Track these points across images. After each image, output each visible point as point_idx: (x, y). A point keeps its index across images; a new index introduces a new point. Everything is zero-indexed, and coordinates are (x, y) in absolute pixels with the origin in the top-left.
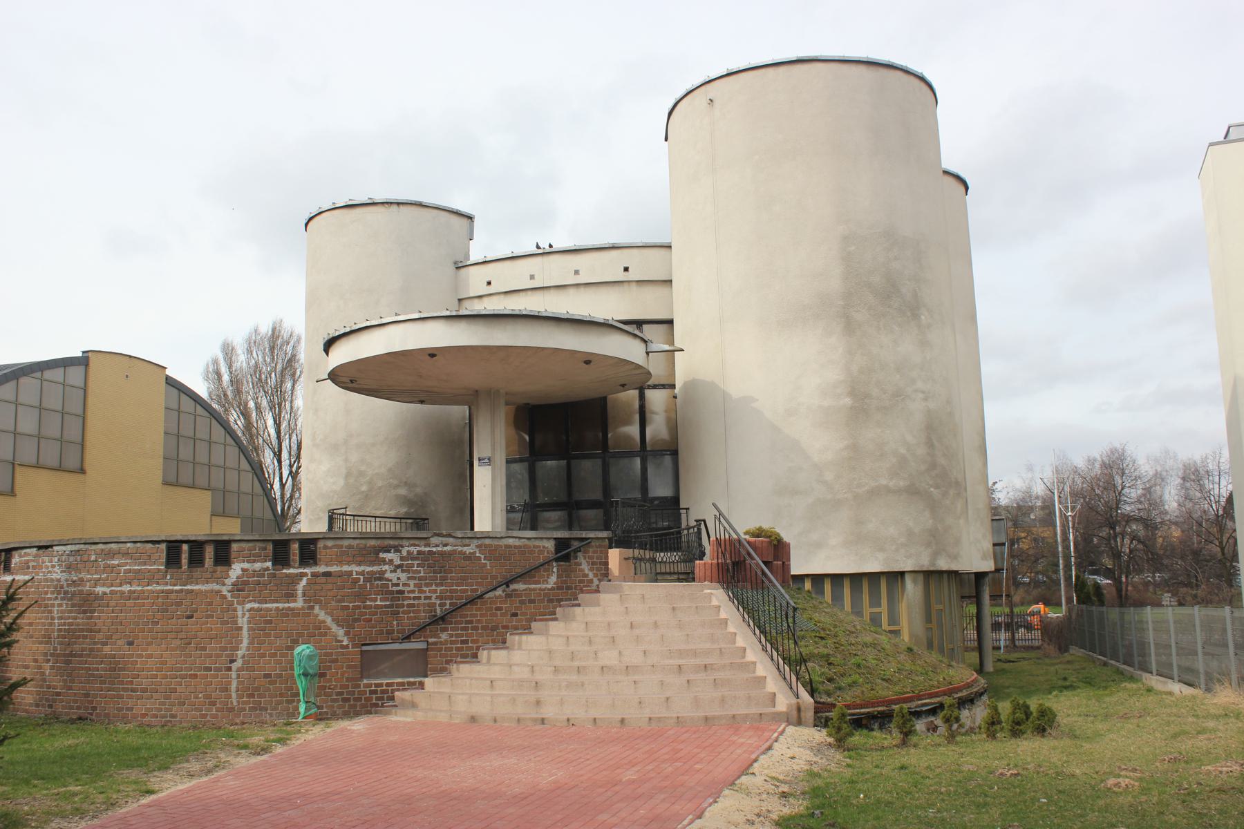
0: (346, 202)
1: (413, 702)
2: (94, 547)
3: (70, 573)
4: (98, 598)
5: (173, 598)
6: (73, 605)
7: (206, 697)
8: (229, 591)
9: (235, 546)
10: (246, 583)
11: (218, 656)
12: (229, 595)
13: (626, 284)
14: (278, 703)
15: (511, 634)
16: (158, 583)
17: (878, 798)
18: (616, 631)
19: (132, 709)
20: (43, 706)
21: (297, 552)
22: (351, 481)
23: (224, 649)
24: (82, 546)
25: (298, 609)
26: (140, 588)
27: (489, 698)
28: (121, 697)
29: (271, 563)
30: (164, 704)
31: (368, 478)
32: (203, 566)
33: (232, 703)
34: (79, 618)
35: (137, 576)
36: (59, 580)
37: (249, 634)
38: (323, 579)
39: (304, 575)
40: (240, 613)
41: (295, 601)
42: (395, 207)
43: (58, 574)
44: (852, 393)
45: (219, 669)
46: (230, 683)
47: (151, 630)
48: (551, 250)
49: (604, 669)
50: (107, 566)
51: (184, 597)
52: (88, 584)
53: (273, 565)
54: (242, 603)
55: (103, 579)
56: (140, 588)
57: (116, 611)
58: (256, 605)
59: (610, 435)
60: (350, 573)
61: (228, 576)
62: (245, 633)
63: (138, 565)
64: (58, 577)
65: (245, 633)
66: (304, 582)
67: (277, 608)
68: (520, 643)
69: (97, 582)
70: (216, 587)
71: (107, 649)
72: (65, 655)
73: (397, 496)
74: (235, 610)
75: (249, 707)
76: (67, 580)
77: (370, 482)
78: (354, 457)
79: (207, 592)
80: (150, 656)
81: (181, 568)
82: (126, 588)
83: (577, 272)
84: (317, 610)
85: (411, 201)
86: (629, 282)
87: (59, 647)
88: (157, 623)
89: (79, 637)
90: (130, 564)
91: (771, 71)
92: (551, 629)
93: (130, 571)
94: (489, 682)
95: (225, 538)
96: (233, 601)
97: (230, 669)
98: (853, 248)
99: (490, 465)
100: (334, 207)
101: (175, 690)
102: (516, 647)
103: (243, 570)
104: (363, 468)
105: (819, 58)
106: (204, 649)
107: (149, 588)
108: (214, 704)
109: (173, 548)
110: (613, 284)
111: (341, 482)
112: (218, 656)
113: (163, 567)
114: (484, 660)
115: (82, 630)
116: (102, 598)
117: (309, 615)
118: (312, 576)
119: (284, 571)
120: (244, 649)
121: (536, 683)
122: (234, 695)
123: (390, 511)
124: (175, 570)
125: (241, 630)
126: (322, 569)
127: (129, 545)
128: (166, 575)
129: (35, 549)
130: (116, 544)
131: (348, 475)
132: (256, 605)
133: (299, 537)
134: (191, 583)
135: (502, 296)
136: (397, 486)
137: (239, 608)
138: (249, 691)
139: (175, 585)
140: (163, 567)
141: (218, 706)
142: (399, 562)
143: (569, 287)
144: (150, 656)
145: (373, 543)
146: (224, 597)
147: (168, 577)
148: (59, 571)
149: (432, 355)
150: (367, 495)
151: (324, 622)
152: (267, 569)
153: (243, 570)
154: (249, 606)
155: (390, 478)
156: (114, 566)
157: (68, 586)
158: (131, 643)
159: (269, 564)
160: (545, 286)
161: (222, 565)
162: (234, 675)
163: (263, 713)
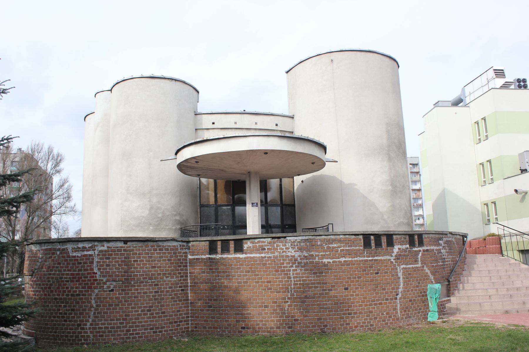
0: (150, 75)
1: (457, 308)
2: (318, 237)
3: (302, 252)
4: (325, 265)
5: (368, 264)
6: (306, 270)
7: (387, 314)
8: (394, 260)
9: (394, 237)
10: (400, 255)
11: (391, 292)
12: (394, 261)
13: (276, 131)
14: (415, 314)
15: (462, 276)
16: (360, 256)
18: (501, 274)
19: (349, 324)
20: (284, 327)
21: (417, 240)
23: (393, 289)
24: (310, 237)
25: (419, 267)
26: (350, 259)
27: (501, 303)
28: (342, 318)
29: (408, 245)
30: (367, 319)
31: (162, 211)
33: (398, 315)
34: (311, 277)
35: (349, 253)
36: (294, 256)
37: (403, 280)
39: (420, 251)
40: (399, 270)
41: (418, 264)
42: (174, 81)
43: (292, 252)
44: (392, 185)
45: (391, 299)
46: (396, 306)
47: (357, 281)
48: (244, 112)
49: (527, 288)
50: (329, 248)
51: (373, 263)
52: (317, 258)
53: (409, 246)
54: (399, 265)
55: (327, 255)
56: (350, 259)
57: (337, 272)
58: (404, 266)
59: (218, 195)
60: (433, 250)
61: (393, 252)
62: (401, 280)
63: (348, 247)
64: (293, 254)
65: (401, 280)
66: (420, 255)
67: (412, 268)
68: (468, 280)
69: (323, 257)
70: (388, 257)
71: (332, 293)
72: (300, 298)
73: (176, 220)
74: (397, 269)
75: (405, 317)
76: (299, 256)
77: (163, 213)
78: (155, 200)
79: (384, 260)
80: (357, 295)
81: (371, 248)
82: (342, 259)
84: (425, 268)
85: (181, 80)
86: (277, 130)
87: (295, 294)
88: (360, 277)
89: (312, 287)
90: (343, 246)
91: (358, 53)
92: (472, 274)
93: (343, 250)
94: (488, 296)
95: (392, 233)
96: (396, 264)
97: (396, 299)
98: (389, 128)
99: (257, 206)
100: (132, 77)
101: (371, 312)
102: (466, 282)
103: (399, 249)
104: (159, 206)
105: (376, 52)
106: (384, 289)
107: (356, 259)
108: (390, 317)
109: (366, 237)
110: (270, 131)
111: (147, 212)
112: (391, 292)
113: (362, 248)
114: (461, 288)
115: (314, 283)
116: (327, 265)
117: (422, 270)
118: (423, 251)
119: (413, 249)
120: (401, 288)
121: (511, 295)
122: (399, 312)
123: (173, 227)
124: (368, 249)
125: (400, 279)
126: (425, 248)
127: (341, 236)
128: (364, 252)
129: (270, 239)
130: (333, 236)
131: (151, 208)
132: (404, 266)
133: (418, 233)
134: (377, 256)
135: (220, 130)
136: (175, 215)
137: (398, 268)
138: (405, 309)
139: (369, 257)
140: (362, 248)
141: (393, 318)
143: (251, 130)
144: (357, 295)
145: (437, 236)
146: (392, 262)
147: (365, 253)
148: (293, 251)
149: (266, 153)
150: (162, 219)
152: (407, 248)
153: (399, 249)
154: (402, 267)
155: (173, 211)
156: (333, 248)
157: (301, 259)
158: (346, 289)
159: (408, 246)
160: (243, 128)
162: (398, 301)
163: (410, 319)
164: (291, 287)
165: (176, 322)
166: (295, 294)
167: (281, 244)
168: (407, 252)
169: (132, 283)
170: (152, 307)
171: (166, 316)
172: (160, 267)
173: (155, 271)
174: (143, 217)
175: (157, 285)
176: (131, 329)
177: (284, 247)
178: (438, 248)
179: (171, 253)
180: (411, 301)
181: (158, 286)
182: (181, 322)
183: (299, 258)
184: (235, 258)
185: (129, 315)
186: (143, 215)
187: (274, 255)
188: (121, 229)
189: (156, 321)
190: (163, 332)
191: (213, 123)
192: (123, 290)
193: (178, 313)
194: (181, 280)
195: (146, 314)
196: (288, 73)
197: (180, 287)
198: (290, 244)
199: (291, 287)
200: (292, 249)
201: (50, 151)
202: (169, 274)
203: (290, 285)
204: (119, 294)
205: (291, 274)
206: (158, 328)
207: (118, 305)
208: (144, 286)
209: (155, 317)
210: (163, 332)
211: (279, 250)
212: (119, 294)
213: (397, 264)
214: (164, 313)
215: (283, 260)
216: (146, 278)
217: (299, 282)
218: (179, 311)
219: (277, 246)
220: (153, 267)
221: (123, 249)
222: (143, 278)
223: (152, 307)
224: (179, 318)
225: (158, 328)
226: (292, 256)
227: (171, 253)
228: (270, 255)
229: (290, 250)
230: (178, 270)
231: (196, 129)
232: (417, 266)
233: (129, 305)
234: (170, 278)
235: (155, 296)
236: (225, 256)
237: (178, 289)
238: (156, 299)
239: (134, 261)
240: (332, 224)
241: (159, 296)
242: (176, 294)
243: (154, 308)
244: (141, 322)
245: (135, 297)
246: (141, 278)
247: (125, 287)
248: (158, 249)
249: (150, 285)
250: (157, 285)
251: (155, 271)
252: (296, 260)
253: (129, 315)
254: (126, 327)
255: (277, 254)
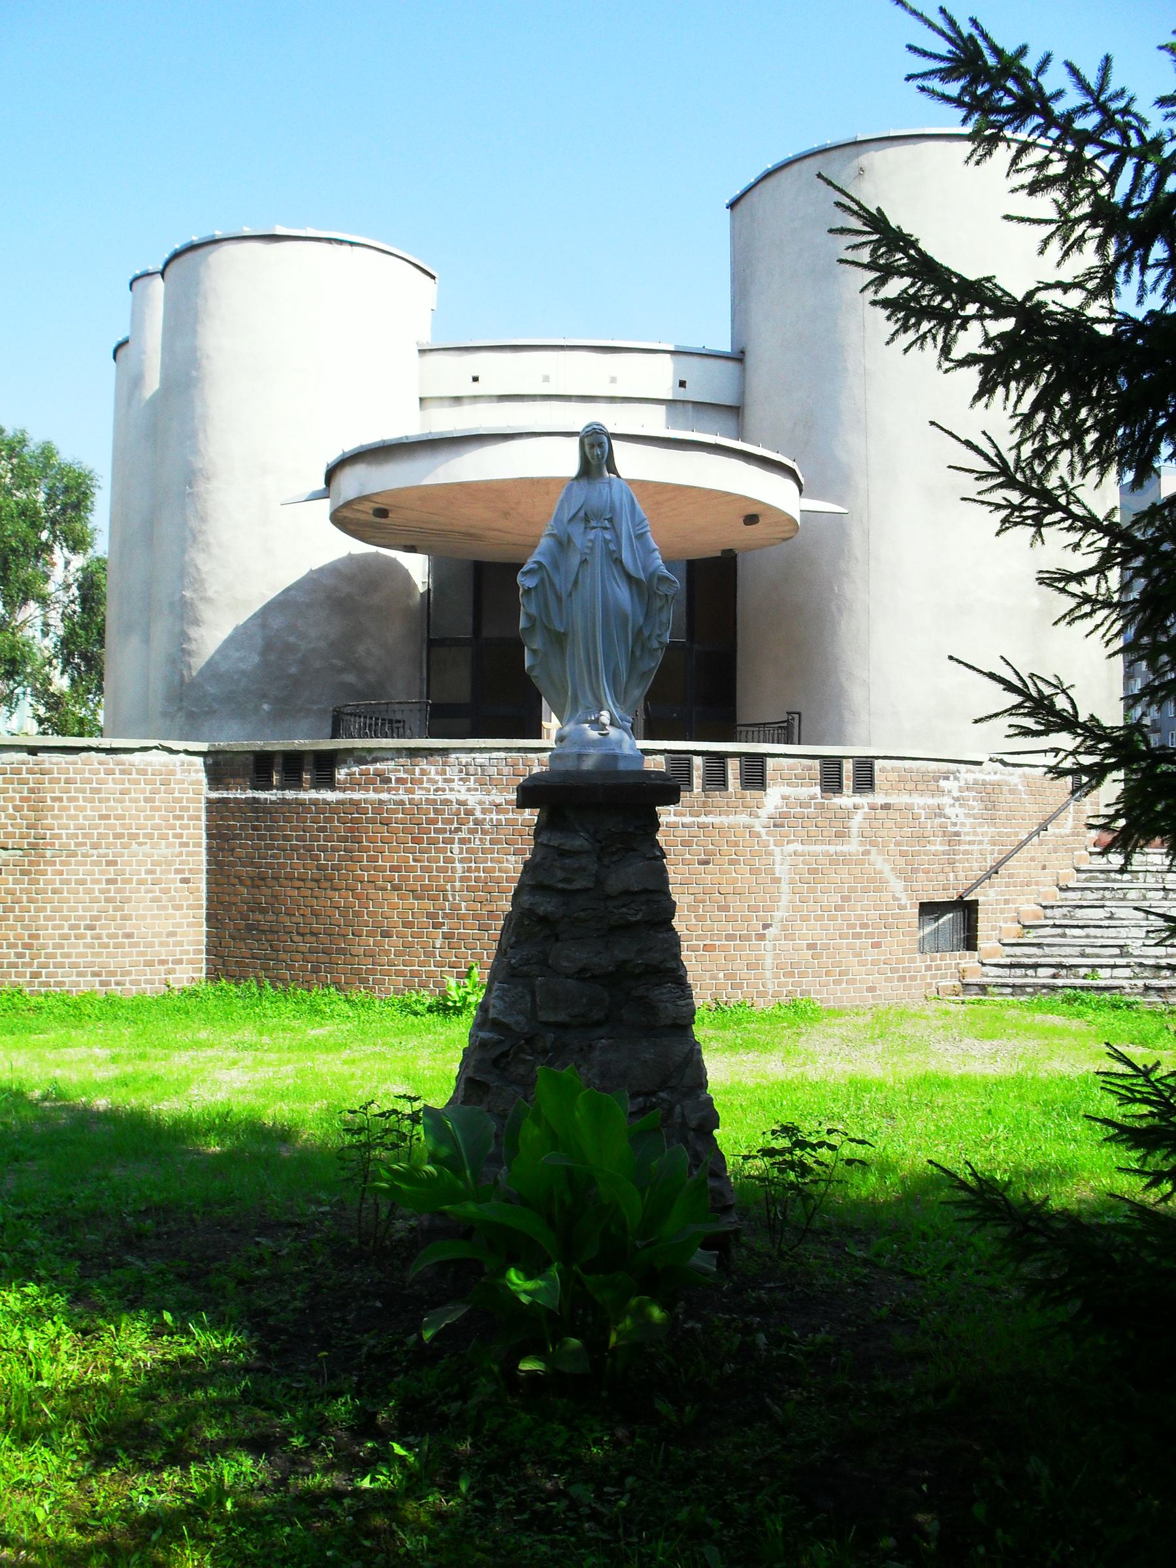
10: (782, 816)
17: (481, 1102)
22: (272, 657)
31: (299, 655)
32: (727, 789)
38: (881, 813)
40: (778, 858)
58: (798, 847)
64: (462, 797)
76: (480, 803)
83: (613, 380)
103: (784, 798)
104: (292, 639)
111: (256, 659)
131: (268, 647)
132: (798, 847)
137: (777, 850)
142: (958, 794)
151: (881, 872)
152: (813, 798)
153: (784, 798)
159: (817, 790)
161: (754, 788)
164: (453, 887)
165: (163, 962)
166: (463, 904)
167: (433, 767)
168: (810, 807)
169: (48, 853)
170: (97, 918)
171: (136, 945)
172: (122, 817)
173: (107, 827)
174: (243, 672)
175: (114, 863)
176: (44, 971)
177: (439, 778)
178: (931, 801)
179: (153, 782)
180: (811, 947)
181: (117, 865)
182: (180, 962)
183: (478, 808)
184: (315, 802)
185: (37, 937)
186: (242, 666)
187: (413, 796)
188: (180, 709)
189: (109, 955)
190: (128, 986)
191: (475, 379)
192: (23, 873)
193: (171, 940)
194: (180, 854)
195: (83, 937)
196: (738, 208)
197: (177, 871)
198: (456, 769)
199: (453, 887)
200: (461, 783)
201: (47, 453)
202: (146, 836)
203: (451, 880)
204: (16, 882)
205: (456, 851)
206: (113, 974)
207: (12, 910)
208: (78, 864)
209: (107, 946)
210: (128, 986)
211: (425, 785)
212: (16, 882)
213: (772, 839)
214: (129, 936)
215: (436, 811)
216: (84, 844)
217: (476, 874)
218: (172, 934)
219: (423, 772)
220: (101, 817)
221: (24, 767)
222: (77, 845)
223: (97, 918)
224: (173, 954)
225: (113, 974)
226: (459, 803)
227: (153, 782)
228: (402, 797)
229: (455, 785)
230: (173, 828)
231: (421, 399)
232: (844, 848)
233: (38, 910)
234: (148, 846)
235: (108, 891)
236: (290, 795)
237: (172, 876)
238: (108, 900)
239: (54, 799)
240: (799, 714)
241: (118, 891)
242: (166, 891)
243: (103, 921)
244: (68, 956)
245: (54, 892)
246: (70, 844)
247: (31, 863)
248: (117, 772)
249: (94, 863)
250: (114, 863)
251: (107, 827)
252: (469, 813)
253: (39, 935)
254: (30, 965)
255: (417, 796)
